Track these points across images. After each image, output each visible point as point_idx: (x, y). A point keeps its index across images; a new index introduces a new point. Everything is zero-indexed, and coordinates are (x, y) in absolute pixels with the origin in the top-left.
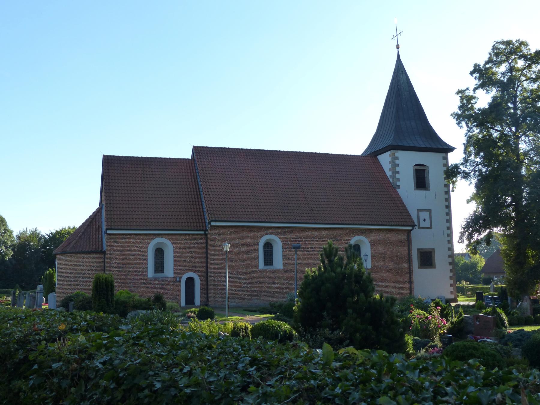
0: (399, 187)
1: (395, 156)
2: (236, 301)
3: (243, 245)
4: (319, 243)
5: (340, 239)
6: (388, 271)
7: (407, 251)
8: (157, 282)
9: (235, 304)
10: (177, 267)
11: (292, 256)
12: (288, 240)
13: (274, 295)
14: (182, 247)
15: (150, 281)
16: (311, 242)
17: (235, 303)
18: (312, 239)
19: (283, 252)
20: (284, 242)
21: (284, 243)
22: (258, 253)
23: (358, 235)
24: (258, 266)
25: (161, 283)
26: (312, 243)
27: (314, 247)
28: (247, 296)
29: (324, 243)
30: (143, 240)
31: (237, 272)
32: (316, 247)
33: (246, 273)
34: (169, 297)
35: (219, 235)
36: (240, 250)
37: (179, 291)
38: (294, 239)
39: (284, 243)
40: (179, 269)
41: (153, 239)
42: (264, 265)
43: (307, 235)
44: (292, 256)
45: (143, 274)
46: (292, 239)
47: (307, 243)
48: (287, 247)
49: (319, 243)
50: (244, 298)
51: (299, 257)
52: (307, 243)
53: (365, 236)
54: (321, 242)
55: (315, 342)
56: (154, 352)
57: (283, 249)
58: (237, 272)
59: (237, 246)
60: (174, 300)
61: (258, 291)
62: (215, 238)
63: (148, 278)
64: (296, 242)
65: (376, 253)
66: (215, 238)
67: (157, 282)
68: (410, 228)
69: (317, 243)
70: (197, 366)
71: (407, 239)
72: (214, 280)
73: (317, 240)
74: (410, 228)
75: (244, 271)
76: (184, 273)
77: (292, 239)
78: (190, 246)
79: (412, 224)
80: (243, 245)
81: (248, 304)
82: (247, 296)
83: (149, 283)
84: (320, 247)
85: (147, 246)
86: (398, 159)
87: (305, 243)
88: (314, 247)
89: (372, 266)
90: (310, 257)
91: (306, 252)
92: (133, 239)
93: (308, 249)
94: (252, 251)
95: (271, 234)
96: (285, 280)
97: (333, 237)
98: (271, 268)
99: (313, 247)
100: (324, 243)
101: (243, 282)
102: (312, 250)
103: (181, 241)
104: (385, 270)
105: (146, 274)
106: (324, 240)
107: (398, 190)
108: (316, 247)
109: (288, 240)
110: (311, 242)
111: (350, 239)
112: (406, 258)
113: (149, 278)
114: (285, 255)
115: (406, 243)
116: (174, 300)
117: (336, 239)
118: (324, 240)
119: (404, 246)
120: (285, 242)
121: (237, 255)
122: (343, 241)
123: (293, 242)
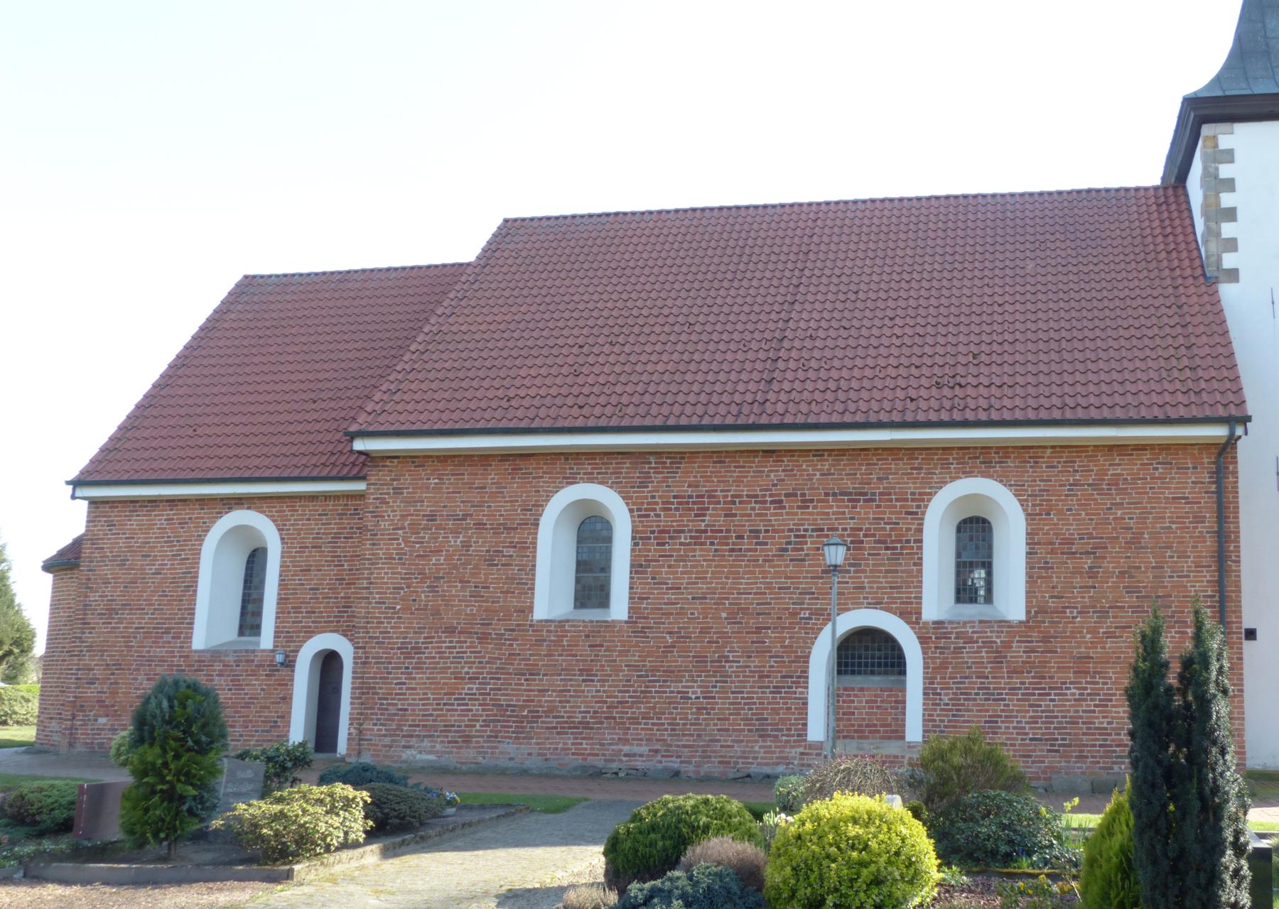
0: (1233, 275)
1: (1216, 146)
2: (438, 747)
4: (787, 514)
5: (881, 494)
6: (1109, 635)
7: (1210, 542)
8: (218, 667)
9: (432, 757)
10: (289, 613)
11: (669, 567)
12: (657, 503)
13: (586, 725)
14: (308, 542)
15: (199, 661)
16: (753, 509)
17: (430, 753)
18: (756, 496)
19: (633, 550)
20: (639, 510)
21: (639, 516)
22: (534, 557)
23: (969, 474)
24: (531, 609)
25: (231, 671)
26: (757, 515)
27: (767, 531)
29: (811, 514)
30: (190, 519)
31: (451, 630)
32: (775, 531)
33: (484, 638)
34: (251, 721)
35: (398, 491)
36: (466, 545)
37: (287, 699)
38: (683, 497)
39: (639, 516)
40: (294, 622)
41: (220, 514)
42: (575, 607)
44: (669, 567)
45: (180, 638)
46: (675, 497)
47: (735, 515)
48: (653, 532)
49: (787, 514)
50: (468, 736)
51: (697, 573)
52: (735, 515)
53: (1002, 479)
54: (799, 507)
58: (451, 630)
60: (267, 731)
61: (524, 707)
62: (384, 502)
63: (191, 651)
64: (690, 509)
65: (1052, 552)
66: (384, 502)
67: (218, 667)
68: (1218, 432)
69: (781, 514)
71: (1213, 488)
73: (781, 501)
74: (1218, 432)
75: (477, 628)
76: (310, 633)
77: (675, 497)
78: (336, 537)
79: (1233, 411)
80: (480, 525)
81: (480, 759)
82: (478, 727)
83: (196, 671)
84: (790, 530)
85: (201, 539)
86: (1232, 161)
87: (726, 515)
88: (767, 531)
89: (1028, 612)
90: (745, 573)
91: (733, 550)
92: (160, 518)
93: (738, 537)
94: (511, 551)
95: (591, 480)
96: (634, 668)
97: (849, 485)
98: (582, 618)
99: (759, 531)
100: (811, 514)
101: (467, 673)
102: (757, 544)
103: (309, 520)
104: (1093, 631)
105: (189, 637)
106: (812, 501)
107: (1227, 291)
108: (775, 531)
109: (657, 503)
111: (930, 494)
112: (1208, 576)
113: (196, 651)
114: (641, 566)
115: (1207, 503)
116: (267, 731)
117: (865, 494)
118: (812, 501)
119: (1199, 519)
120: (646, 510)
121: (455, 567)
122: (897, 500)
123: (677, 509)
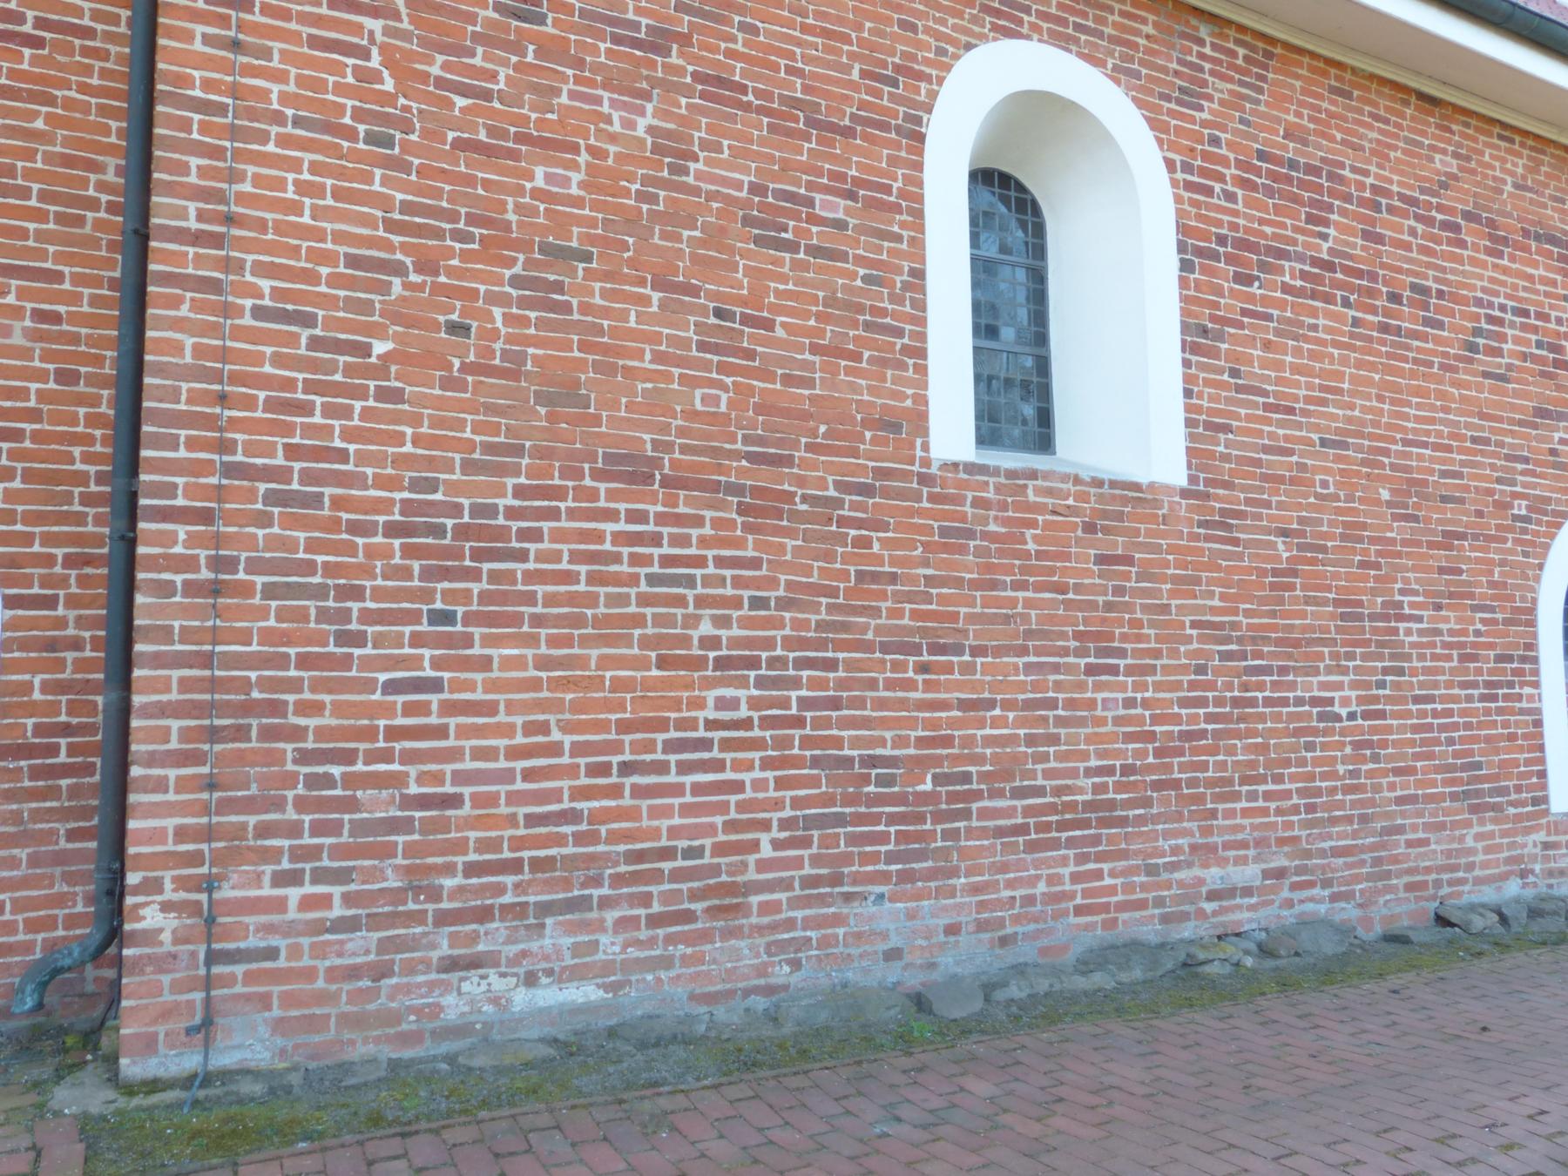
3: (717, 86)
9: (587, 993)
11: (1267, 345)
17: (576, 974)
20: (1187, 168)
21: (1189, 186)
24: (919, 420)
28: (767, 851)
39: (1189, 186)
43: (1380, 154)
47: (1379, 239)
48: (1222, 240)
50: (731, 889)
52: (1379, 239)
55: (535, 1092)
56: (695, 635)
57: (1182, 247)
59: (633, 92)
70: (463, 363)
72: (216, 589)
73: (1456, 228)
75: (736, 471)
80: (717, 86)
81: (782, 973)
101: (710, 642)
110: (1413, 232)
114: (1205, 332)
121: (631, 221)
